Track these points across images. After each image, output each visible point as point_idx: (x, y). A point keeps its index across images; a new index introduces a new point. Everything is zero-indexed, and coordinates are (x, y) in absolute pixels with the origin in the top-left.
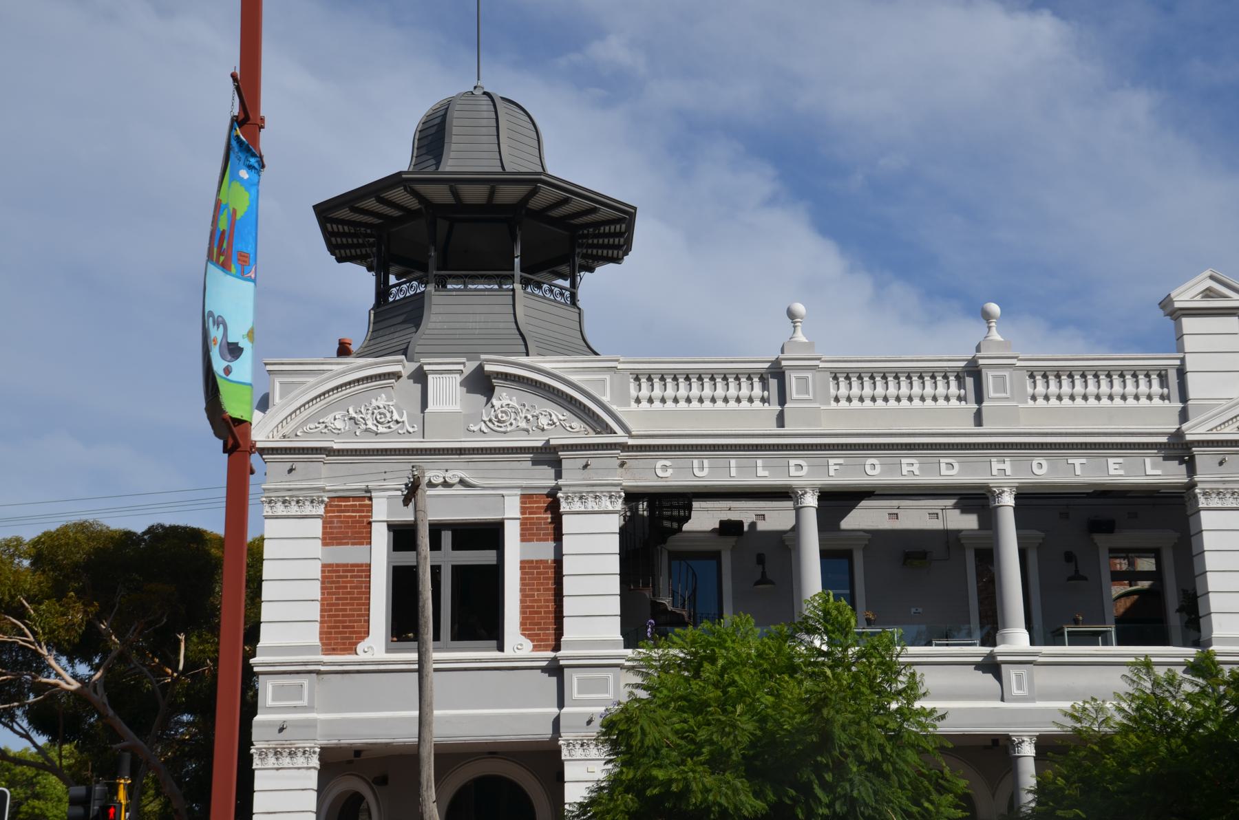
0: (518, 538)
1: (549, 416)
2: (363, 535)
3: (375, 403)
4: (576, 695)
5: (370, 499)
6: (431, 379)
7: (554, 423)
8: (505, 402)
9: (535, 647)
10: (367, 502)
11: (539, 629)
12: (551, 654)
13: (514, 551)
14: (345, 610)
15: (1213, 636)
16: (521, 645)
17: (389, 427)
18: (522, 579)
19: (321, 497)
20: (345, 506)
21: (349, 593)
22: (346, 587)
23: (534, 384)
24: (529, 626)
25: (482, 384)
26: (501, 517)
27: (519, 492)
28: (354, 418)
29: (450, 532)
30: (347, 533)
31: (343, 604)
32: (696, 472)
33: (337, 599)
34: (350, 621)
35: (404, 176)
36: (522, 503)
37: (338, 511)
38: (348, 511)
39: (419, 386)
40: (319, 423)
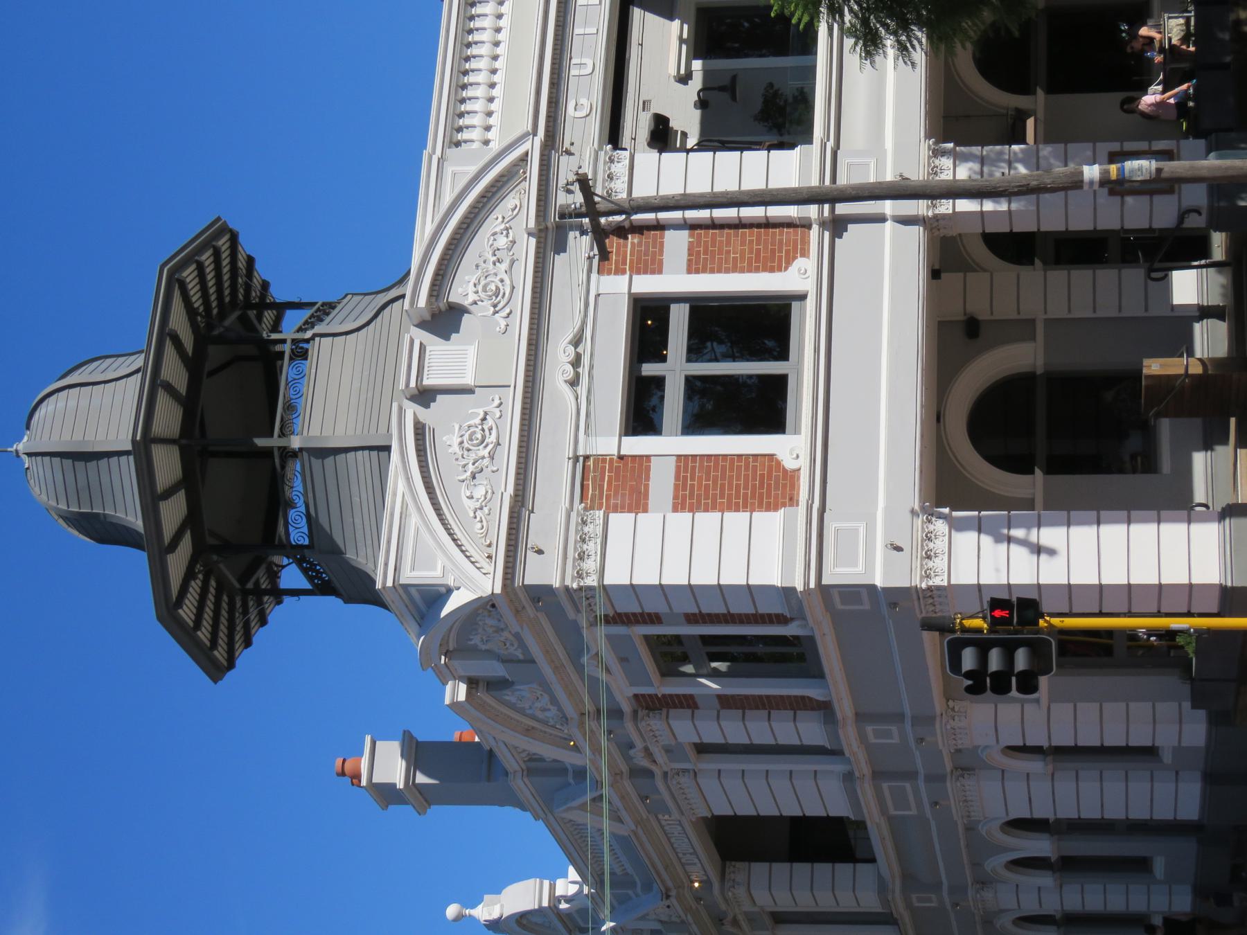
0: (656, 277)
1: (495, 237)
3: (456, 448)
4: (860, 568)
5: (587, 458)
6: (428, 381)
7: (507, 229)
8: (471, 288)
9: (803, 255)
10: (591, 463)
11: (780, 251)
12: (815, 228)
14: (738, 486)
15: (779, 585)
16: (799, 270)
17: (490, 429)
18: (712, 271)
19: (578, 511)
20: (594, 472)
21: (715, 482)
23: (455, 242)
24: (775, 263)
26: (627, 296)
27: (594, 276)
28: (472, 473)
29: (644, 365)
30: (631, 486)
31: (730, 489)
33: (722, 497)
34: (754, 479)
35: (138, 438)
36: (609, 273)
37: (601, 498)
38: (601, 487)
39: (439, 397)
40: (475, 517)
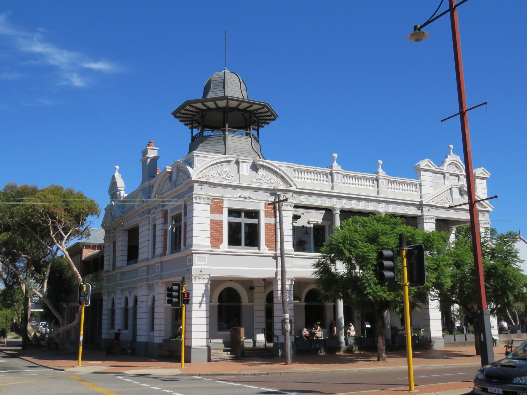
2: (221, 212)
3: (225, 170)
4: (196, 263)
6: (241, 163)
8: (262, 174)
9: (269, 249)
10: (222, 201)
12: (275, 252)
13: (264, 221)
17: (230, 178)
21: (217, 229)
22: (216, 227)
24: (267, 243)
25: (255, 168)
27: (264, 202)
31: (215, 233)
32: (352, 205)
35: (228, 97)
38: (216, 203)
39: (237, 166)
